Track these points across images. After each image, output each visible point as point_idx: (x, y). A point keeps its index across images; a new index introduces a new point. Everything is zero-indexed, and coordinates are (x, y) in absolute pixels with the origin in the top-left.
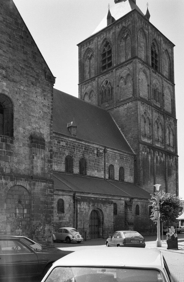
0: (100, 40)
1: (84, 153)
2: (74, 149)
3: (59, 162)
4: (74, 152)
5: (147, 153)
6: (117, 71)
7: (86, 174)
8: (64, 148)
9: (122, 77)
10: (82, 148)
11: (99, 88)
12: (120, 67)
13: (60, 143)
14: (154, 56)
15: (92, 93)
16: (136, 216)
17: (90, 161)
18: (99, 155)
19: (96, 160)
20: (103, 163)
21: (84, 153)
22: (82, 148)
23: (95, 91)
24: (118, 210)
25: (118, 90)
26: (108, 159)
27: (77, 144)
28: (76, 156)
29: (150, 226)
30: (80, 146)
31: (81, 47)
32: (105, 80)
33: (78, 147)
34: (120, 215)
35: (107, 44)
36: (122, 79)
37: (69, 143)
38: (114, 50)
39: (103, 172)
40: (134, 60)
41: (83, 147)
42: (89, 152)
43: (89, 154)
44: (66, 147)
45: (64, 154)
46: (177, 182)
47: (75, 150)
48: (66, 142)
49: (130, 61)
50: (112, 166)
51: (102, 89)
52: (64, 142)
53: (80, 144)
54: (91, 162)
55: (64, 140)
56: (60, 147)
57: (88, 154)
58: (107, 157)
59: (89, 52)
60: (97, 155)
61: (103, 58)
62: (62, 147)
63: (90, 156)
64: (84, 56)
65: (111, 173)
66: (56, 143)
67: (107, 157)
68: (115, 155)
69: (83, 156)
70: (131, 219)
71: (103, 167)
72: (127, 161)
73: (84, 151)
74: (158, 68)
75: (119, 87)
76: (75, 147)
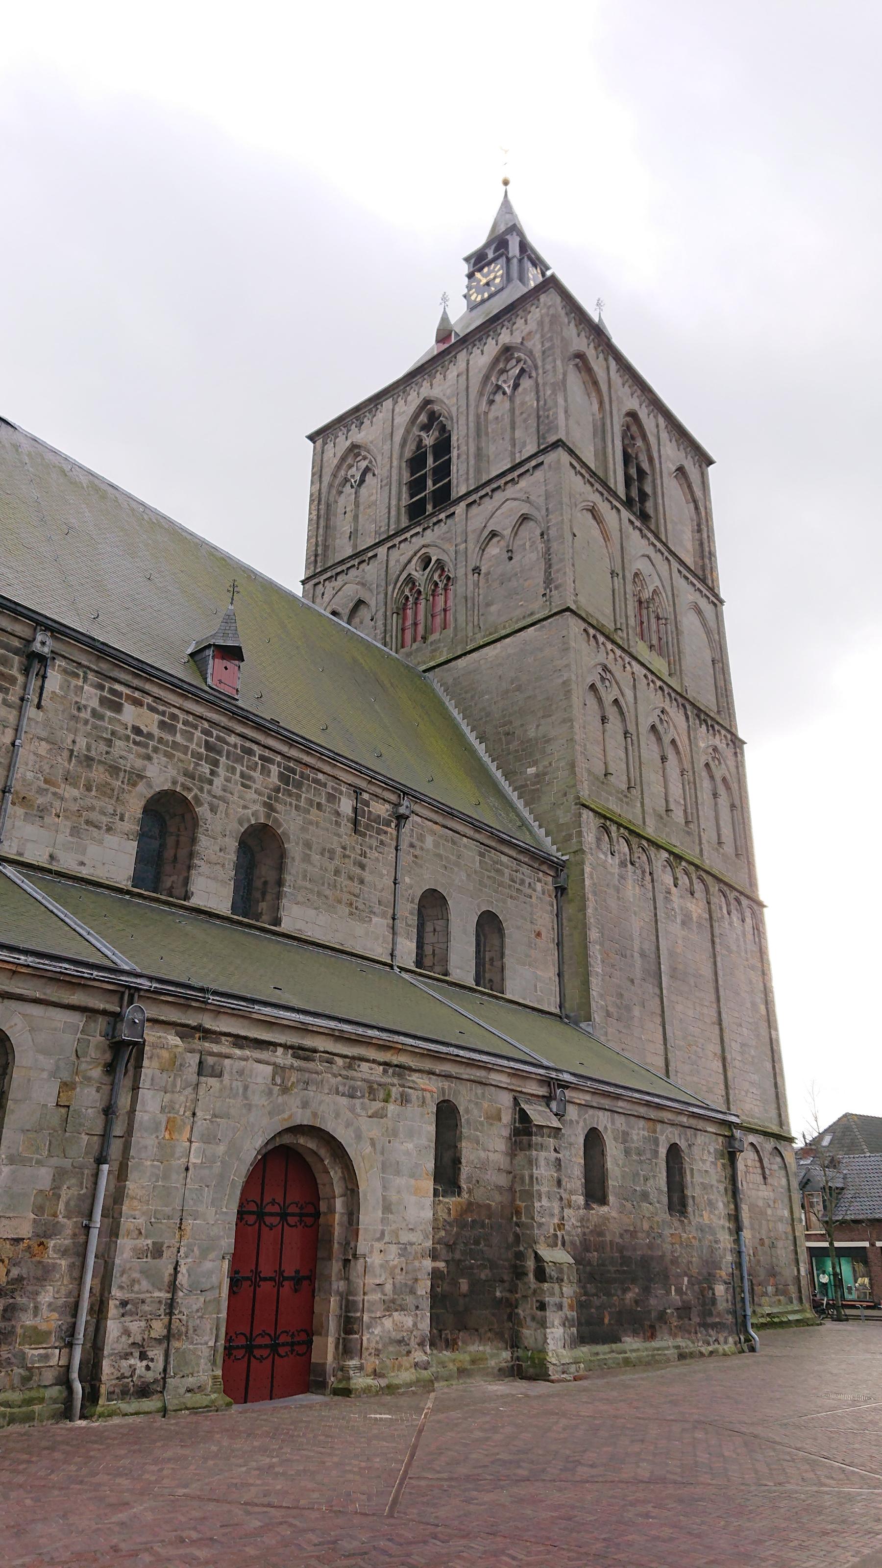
0: (406, 408)
1: (277, 799)
2: (216, 763)
3: (94, 816)
4: (211, 783)
5: (623, 864)
6: (474, 510)
7: (277, 922)
8: (146, 746)
9: (493, 534)
10: (265, 772)
11: (390, 588)
12: (487, 494)
13: (117, 708)
14: (633, 471)
15: (363, 612)
16: (587, 1206)
17: (310, 849)
18: (368, 827)
19: (344, 848)
20: (387, 871)
21: (277, 799)
22: (265, 772)
23: (373, 603)
24: (469, 1153)
25: (477, 585)
26: (416, 857)
27: (232, 739)
28: (222, 807)
29: (679, 1291)
30: (257, 759)
31: (325, 443)
32: (419, 555)
33: (239, 760)
34: (479, 1195)
35: (431, 417)
36: (495, 540)
37: (180, 726)
38: (463, 432)
39: (380, 923)
40: (549, 458)
41: (274, 769)
42: (310, 802)
43: (308, 812)
44: (161, 740)
45: (141, 777)
46: (773, 1032)
47: (221, 771)
48: (163, 714)
49: (533, 463)
50: (433, 903)
51: (403, 592)
52: (152, 709)
53: (255, 747)
54: (316, 858)
55: (149, 700)
56: (113, 733)
57: (297, 808)
58: (412, 846)
59: (358, 459)
60: (355, 822)
61: (412, 475)
62: (127, 738)
63: (311, 823)
64: (335, 475)
65: (429, 938)
66: (94, 703)
67: (412, 846)
68: (454, 843)
69: (268, 816)
70: (561, 1226)
71: (388, 896)
72: (517, 886)
73: (277, 790)
74: (653, 521)
75: (479, 574)
76: (219, 753)
